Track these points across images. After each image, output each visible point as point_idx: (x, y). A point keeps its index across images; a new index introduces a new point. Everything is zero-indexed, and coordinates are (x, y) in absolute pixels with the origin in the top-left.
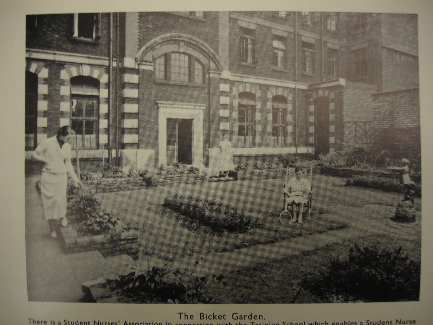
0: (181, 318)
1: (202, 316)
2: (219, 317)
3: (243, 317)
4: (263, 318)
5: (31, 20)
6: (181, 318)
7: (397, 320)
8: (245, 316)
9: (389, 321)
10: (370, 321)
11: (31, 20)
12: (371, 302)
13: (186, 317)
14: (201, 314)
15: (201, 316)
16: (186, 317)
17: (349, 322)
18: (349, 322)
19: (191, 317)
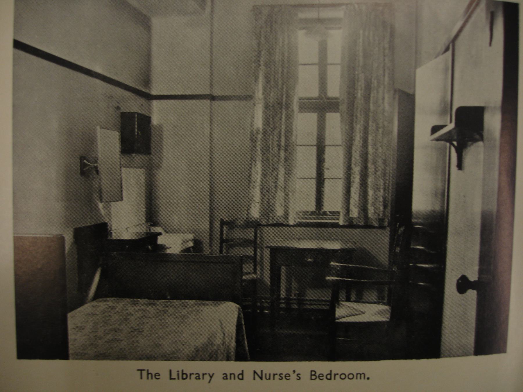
0: (490, 44)
1: (313, 375)
2: (285, 376)
3: (201, 377)
4: (366, 377)
5: (27, 350)
6: (490, 44)
7: (255, 372)
8: (274, 375)
9: (279, 373)
10: (284, 374)
11: (27, 350)
12: (301, 361)
13: (150, 375)
14: (312, 371)
15: (311, 375)
16: (150, 375)
17: (262, 371)
18: (262, 371)
19: (225, 377)
